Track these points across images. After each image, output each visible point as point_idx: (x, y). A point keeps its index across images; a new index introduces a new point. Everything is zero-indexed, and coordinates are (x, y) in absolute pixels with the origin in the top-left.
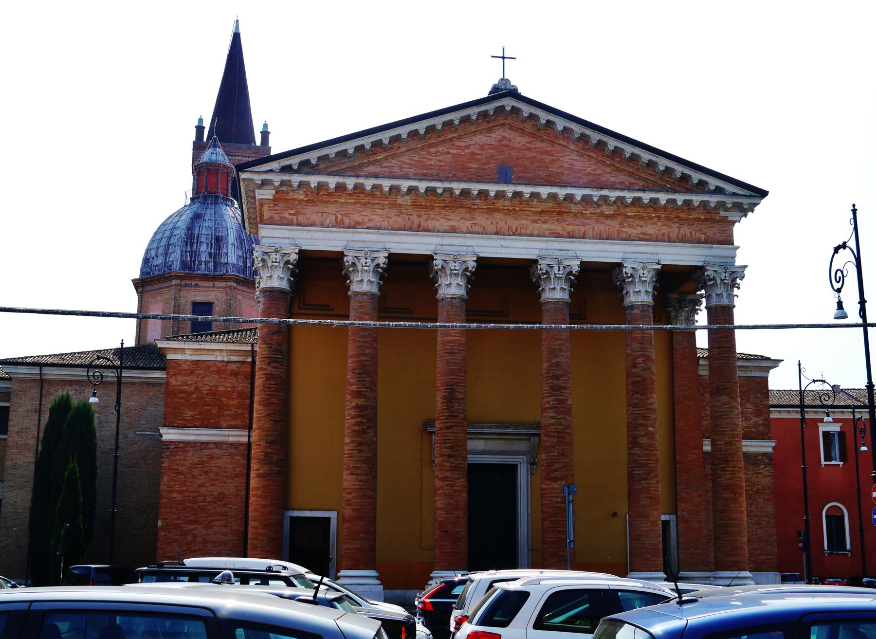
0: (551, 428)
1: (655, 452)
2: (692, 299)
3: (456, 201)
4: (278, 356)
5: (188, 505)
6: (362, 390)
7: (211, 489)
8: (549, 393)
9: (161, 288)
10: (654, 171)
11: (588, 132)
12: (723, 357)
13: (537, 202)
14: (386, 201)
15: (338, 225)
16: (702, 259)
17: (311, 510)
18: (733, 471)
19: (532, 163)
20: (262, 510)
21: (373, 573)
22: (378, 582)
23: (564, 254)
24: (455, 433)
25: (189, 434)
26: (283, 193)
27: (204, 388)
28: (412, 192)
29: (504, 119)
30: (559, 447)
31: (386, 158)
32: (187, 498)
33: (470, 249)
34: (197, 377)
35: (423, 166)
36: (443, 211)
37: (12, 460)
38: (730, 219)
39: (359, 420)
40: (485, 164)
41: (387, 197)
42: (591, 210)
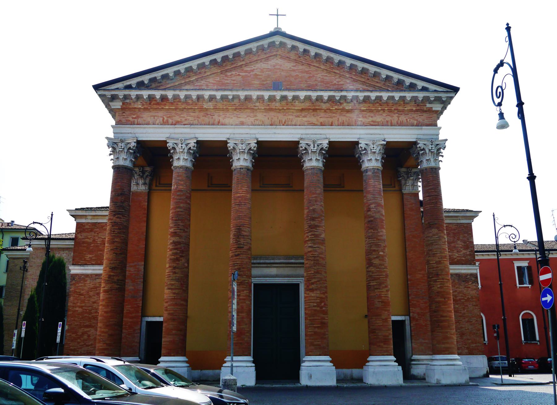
0: (310, 254)
1: (385, 270)
2: (416, 172)
3: (243, 105)
4: (121, 210)
8: (308, 230)
12: (433, 202)
13: (298, 103)
14: (196, 106)
15: (165, 123)
16: (416, 136)
18: (441, 282)
19: (296, 79)
23: (318, 137)
24: (242, 259)
25: (88, 269)
26: (127, 104)
28: (213, 100)
31: (197, 80)
32: (85, 311)
34: (95, 233)
36: (235, 112)
39: (175, 251)
42: (336, 107)
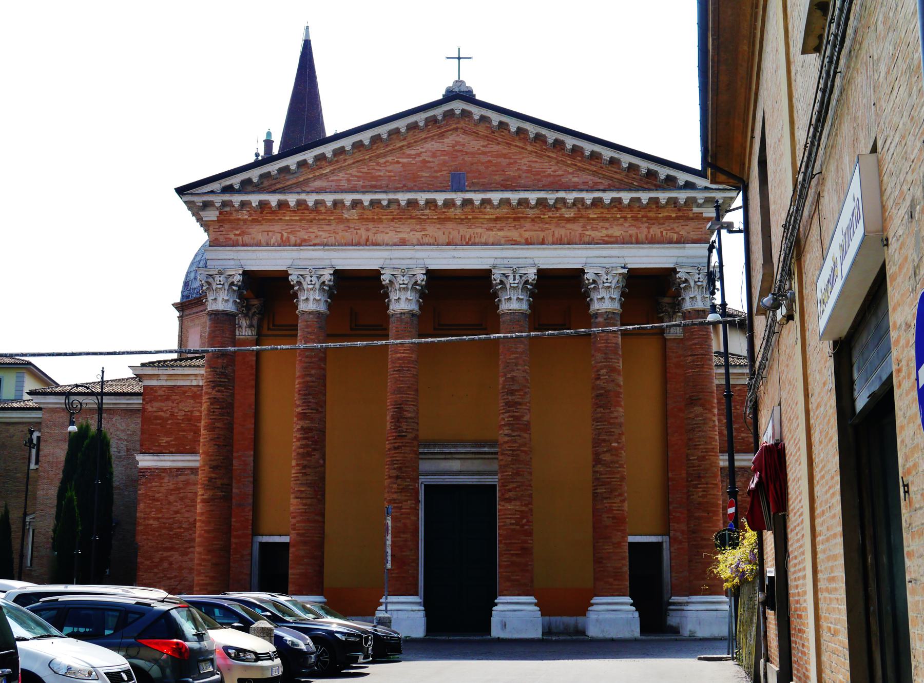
1: (619, 469)
3: (403, 212)
5: (164, 531)
6: (307, 411)
7: (186, 515)
9: (199, 312)
10: (619, 168)
11: (544, 131)
13: (490, 208)
14: (332, 216)
15: (284, 243)
17: (280, 535)
19: (487, 167)
20: (206, 535)
21: (531, 599)
22: (634, 608)
23: (520, 262)
24: (404, 453)
25: (165, 460)
27: (179, 414)
29: (456, 124)
30: (514, 466)
31: (332, 172)
32: (162, 525)
33: (421, 262)
35: (372, 177)
36: (392, 224)
37: (44, 489)
38: (704, 215)
39: (304, 442)
40: (436, 172)
41: (332, 213)
42: (550, 214)
